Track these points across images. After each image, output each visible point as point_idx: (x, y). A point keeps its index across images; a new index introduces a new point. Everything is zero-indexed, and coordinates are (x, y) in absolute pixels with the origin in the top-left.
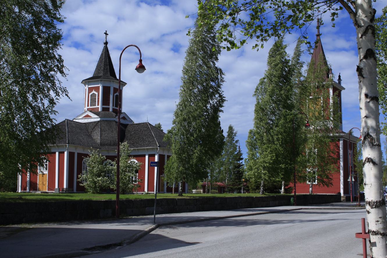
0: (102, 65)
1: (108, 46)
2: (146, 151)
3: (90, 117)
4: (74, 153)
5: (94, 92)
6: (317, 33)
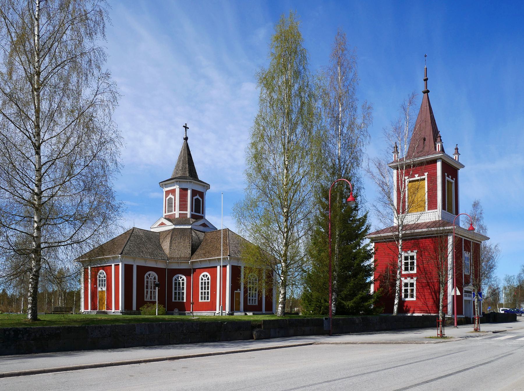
0: (181, 164)
2: (199, 263)
3: (208, 227)
4: (132, 266)
6: (424, 89)
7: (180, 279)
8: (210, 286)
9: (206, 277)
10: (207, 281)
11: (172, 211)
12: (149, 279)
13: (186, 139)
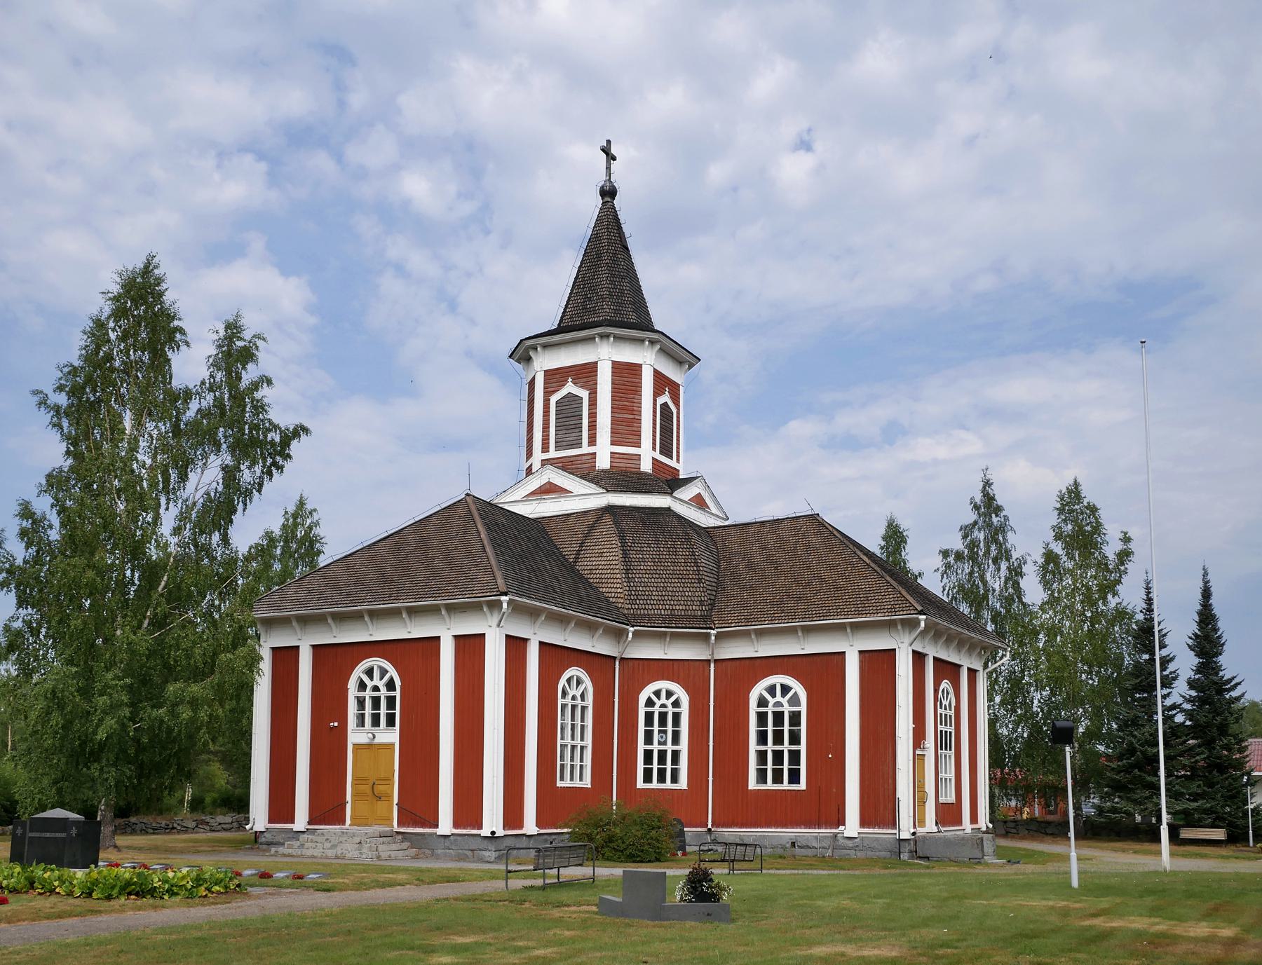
1: (617, 202)
5: (570, 388)
7: (659, 699)
8: (397, 712)
9: (381, 678)
10: (787, 709)
11: (579, 445)
12: (770, 705)
13: (608, 193)
